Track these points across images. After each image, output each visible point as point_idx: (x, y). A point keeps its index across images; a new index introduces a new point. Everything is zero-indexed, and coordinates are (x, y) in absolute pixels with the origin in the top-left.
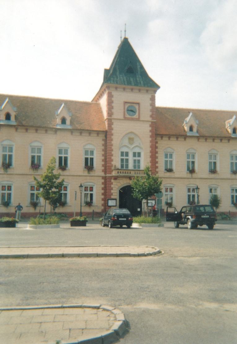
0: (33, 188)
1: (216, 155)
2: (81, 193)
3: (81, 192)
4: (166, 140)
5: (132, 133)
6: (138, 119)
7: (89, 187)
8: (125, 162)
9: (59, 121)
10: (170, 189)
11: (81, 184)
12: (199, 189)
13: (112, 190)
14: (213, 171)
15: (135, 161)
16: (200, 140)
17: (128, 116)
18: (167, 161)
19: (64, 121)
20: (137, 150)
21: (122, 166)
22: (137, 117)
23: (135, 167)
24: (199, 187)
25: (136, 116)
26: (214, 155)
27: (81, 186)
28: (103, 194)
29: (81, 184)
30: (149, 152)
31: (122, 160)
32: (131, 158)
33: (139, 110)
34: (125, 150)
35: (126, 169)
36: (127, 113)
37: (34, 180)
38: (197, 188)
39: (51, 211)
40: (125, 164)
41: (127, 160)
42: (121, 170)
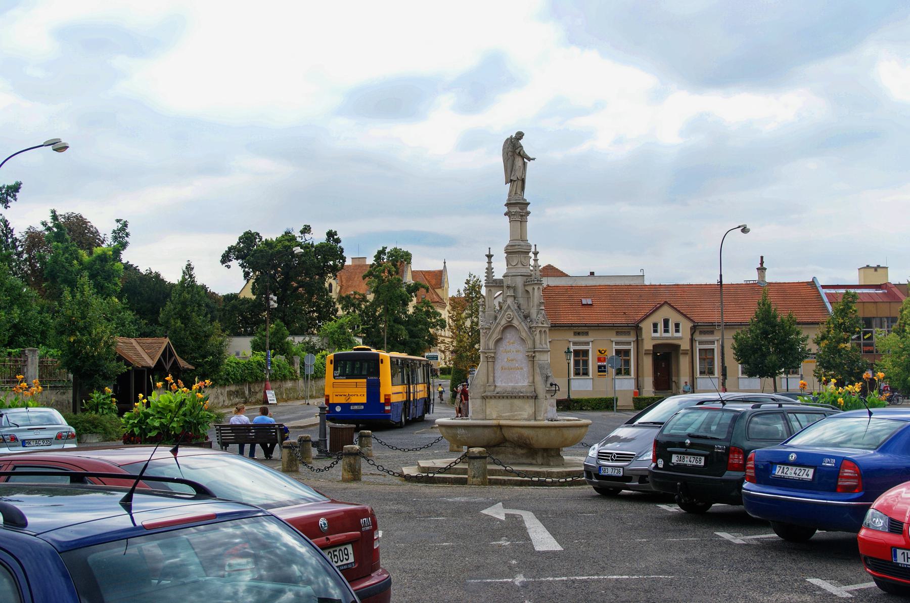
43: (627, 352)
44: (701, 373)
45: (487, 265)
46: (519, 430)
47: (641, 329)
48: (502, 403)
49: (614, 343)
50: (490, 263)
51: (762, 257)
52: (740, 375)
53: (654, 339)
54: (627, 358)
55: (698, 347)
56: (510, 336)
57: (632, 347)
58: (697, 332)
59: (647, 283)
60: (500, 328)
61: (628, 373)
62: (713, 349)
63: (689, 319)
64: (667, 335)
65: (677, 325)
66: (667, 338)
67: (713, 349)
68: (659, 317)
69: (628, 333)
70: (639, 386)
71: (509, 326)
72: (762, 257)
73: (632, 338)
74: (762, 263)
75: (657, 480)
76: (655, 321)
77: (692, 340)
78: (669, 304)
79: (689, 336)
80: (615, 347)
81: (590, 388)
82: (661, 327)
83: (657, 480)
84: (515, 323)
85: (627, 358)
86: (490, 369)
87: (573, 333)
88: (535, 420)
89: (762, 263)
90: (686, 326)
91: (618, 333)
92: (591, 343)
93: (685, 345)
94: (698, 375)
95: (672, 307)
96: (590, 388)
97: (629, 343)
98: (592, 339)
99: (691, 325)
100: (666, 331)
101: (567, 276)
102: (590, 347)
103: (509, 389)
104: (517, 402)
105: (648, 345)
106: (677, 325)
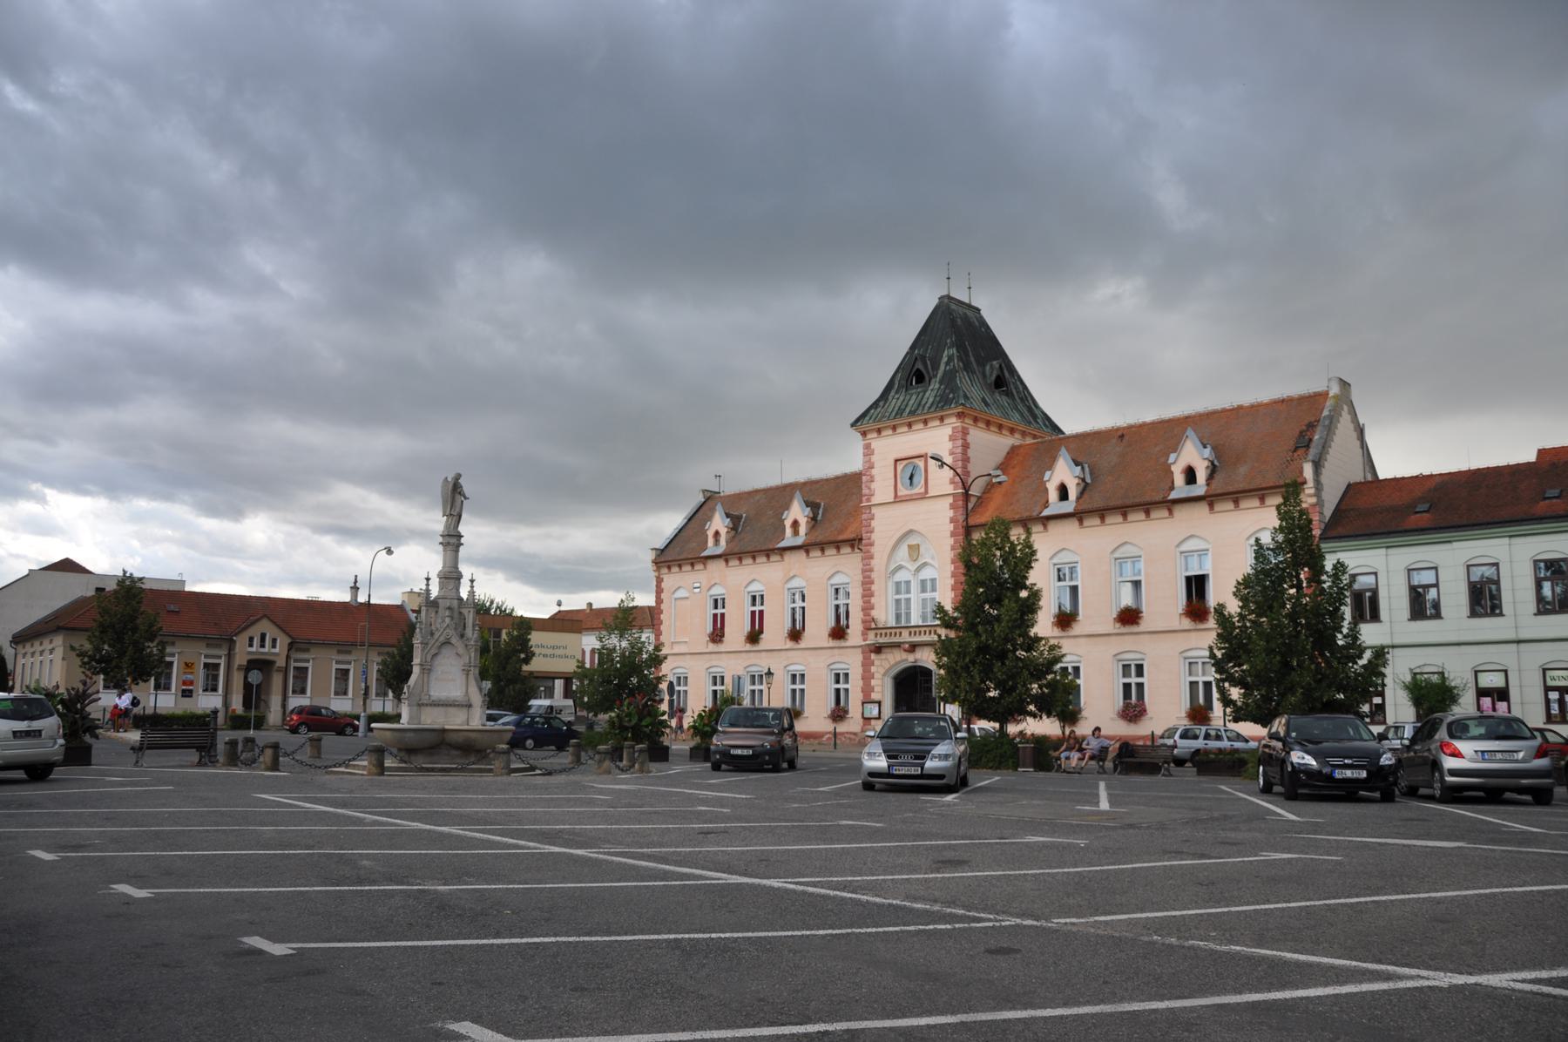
0: (298, 689)
1: (1075, 565)
2: (769, 689)
4: (763, 563)
5: (910, 532)
6: (923, 497)
7: (1133, 664)
8: (901, 608)
9: (1179, 479)
10: (191, 691)
11: (769, 669)
12: (773, 674)
13: (873, 678)
14: (795, 635)
16: (1086, 523)
19: (1063, 493)
22: (923, 490)
24: (772, 671)
25: (919, 489)
26: (1069, 565)
29: (769, 669)
30: (950, 575)
33: (926, 471)
38: (769, 673)
39: (1063, 733)
41: (908, 601)
42: (895, 628)
43: (217, 666)
44: (294, 692)
45: (469, 589)
46: (466, 734)
47: (234, 642)
48: (436, 710)
49: (334, 662)
50: (472, 587)
51: (356, 576)
52: (332, 696)
53: (250, 653)
54: (216, 673)
55: (293, 664)
56: (446, 651)
57: (222, 662)
58: (293, 650)
59: (187, 589)
60: (438, 644)
61: (215, 689)
62: (307, 668)
63: (287, 634)
64: (262, 650)
65: (274, 641)
66: (262, 653)
67: (307, 668)
68: (255, 631)
69: (219, 646)
70: (226, 703)
71: (447, 643)
72: (356, 576)
73: (223, 652)
74: (356, 582)
75: (1046, 727)
76: (251, 635)
77: (288, 657)
78: (269, 618)
79: (286, 653)
80: (203, 660)
81: (172, 704)
82: (256, 641)
83: (1046, 727)
84: (454, 641)
85: (216, 673)
86: (425, 680)
87: (205, 645)
88: (468, 725)
89: (356, 582)
90: (283, 642)
91: (208, 645)
92: (311, 661)
93: (281, 662)
94: (374, 697)
95: (272, 621)
96: (172, 704)
97: (220, 657)
98: (313, 656)
99: (290, 641)
100: (263, 646)
101: (90, 573)
102: (310, 665)
103: (443, 698)
104: (452, 710)
105: (240, 659)
106: (274, 641)
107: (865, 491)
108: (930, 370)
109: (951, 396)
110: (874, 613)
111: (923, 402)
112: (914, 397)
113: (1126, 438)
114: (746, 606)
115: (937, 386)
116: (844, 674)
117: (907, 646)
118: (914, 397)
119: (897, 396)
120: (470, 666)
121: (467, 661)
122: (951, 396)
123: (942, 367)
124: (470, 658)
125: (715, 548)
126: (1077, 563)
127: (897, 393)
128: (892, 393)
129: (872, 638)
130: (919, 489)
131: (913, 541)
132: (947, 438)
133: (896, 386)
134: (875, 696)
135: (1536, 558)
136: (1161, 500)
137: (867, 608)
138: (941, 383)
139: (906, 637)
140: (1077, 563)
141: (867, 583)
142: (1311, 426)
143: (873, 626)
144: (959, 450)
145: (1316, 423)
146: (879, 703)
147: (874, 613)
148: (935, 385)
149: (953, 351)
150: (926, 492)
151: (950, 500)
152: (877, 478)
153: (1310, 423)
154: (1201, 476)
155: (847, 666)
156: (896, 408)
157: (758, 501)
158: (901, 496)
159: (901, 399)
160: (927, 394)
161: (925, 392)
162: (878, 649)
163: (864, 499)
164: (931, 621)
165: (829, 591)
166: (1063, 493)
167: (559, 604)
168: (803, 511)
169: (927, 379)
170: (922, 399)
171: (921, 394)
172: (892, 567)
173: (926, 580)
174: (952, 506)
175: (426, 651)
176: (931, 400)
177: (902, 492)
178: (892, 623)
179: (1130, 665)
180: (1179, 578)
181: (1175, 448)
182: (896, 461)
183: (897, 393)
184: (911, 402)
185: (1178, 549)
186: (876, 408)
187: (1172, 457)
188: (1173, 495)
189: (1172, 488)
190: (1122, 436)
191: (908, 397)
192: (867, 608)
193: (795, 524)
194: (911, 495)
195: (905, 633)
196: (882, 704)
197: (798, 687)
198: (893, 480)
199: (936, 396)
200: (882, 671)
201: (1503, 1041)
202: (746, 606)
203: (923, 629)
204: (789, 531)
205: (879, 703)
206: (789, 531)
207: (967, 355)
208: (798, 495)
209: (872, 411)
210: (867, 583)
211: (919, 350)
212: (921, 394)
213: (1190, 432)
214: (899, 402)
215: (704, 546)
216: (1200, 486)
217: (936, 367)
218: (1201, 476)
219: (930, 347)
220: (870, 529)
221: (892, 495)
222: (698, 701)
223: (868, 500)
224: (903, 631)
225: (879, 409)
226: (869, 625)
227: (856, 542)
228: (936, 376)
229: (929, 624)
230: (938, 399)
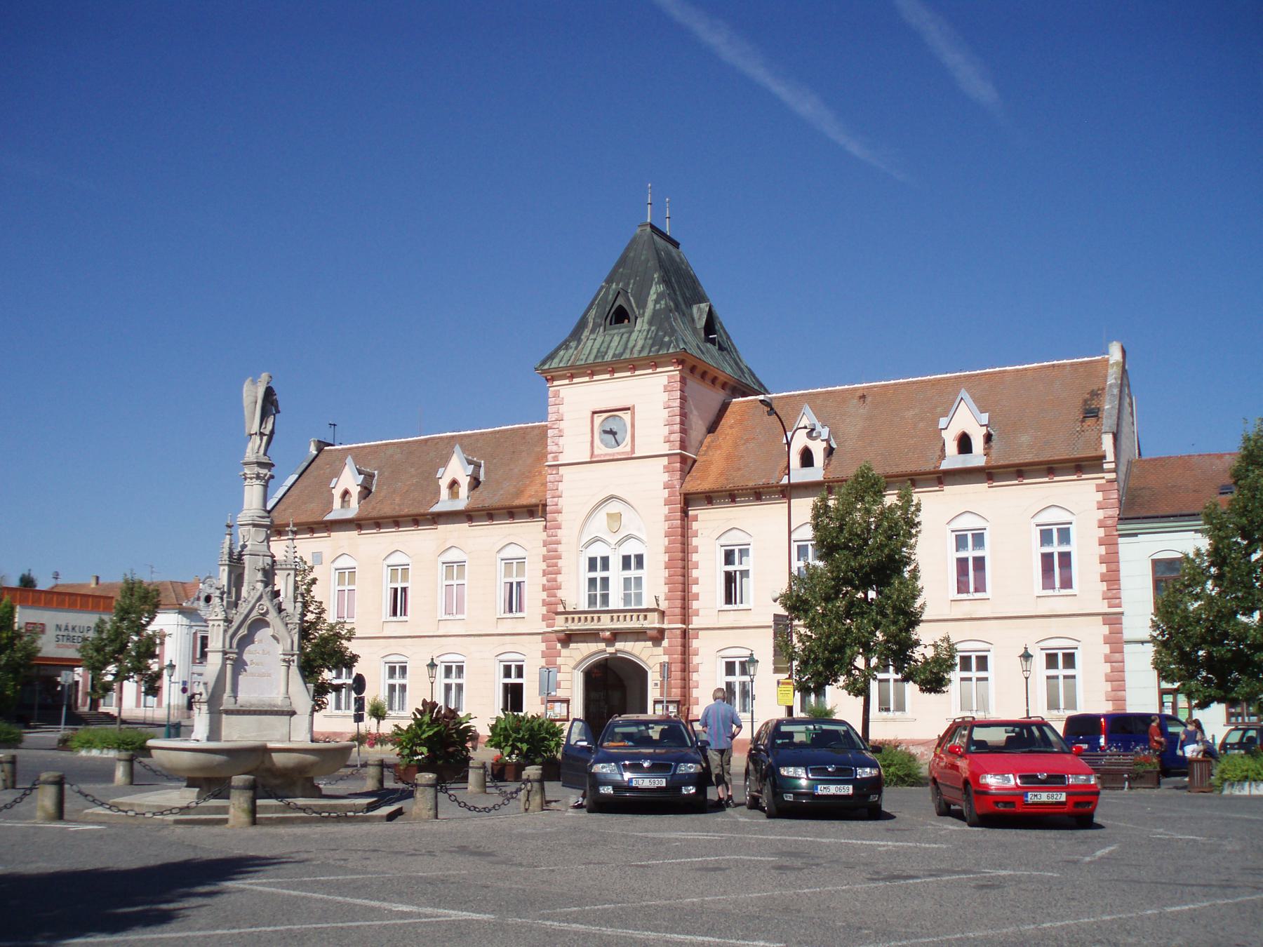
3: (432, 680)
9: (951, 447)
15: (627, 581)
17: (601, 450)
18: (1051, 555)
20: (631, 549)
21: (592, 599)
22: (628, 449)
23: (627, 598)
24: (755, 657)
25: (624, 448)
27: (432, 665)
28: (1108, 660)
31: (592, 582)
32: (616, 574)
33: (633, 426)
34: (598, 551)
35: (590, 609)
36: (602, 441)
37: (210, 655)
40: (599, 592)
41: (605, 581)
107: (551, 448)
108: (635, 309)
109: (667, 339)
110: (561, 594)
111: (630, 345)
112: (616, 339)
113: (869, 399)
114: (439, 580)
115: (646, 327)
116: (516, 666)
117: (608, 634)
118: (616, 339)
119: (593, 336)
120: (293, 655)
121: (289, 647)
122: (667, 339)
123: (650, 305)
124: (292, 642)
125: (343, 510)
126: (1071, 523)
127: (592, 331)
128: (586, 333)
129: (560, 624)
130: (624, 448)
131: (614, 507)
132: (662, 389)
133: (591, 325)
134: (561, 693)
135: (1155, 557)
136: (932, 470)
137: (551, 588)
138: (650, 323)
139: (606, 623)
140: (1071, 523)
141: (552, 560)
142: (1095, 394)
143: (561, 609)
144: (677, 403)
145: (1099, 392)
146: (567, 701)
147: (561, 594)
148: (641, 325)
149: (661, 288)
150: (633, 451)
151: (665, 461)
152: (566, 433)
153: (1093, 391)
154: (978, 444)
155: (521, 657)
156: (595, 351)
157: (392, 456)
158: (598, 456)
159: (599, 340)
160: (634, 336)
161: (631, 333)
162: (568, 638)
163: (550, 456)
164: (635, 605)
165: (332, 577)
166: (965, 444)
167: (56, 576)
168: (465, 469)
169: (632, 318)
170: (628, 341)
171: (625, 336)
172: (585, 539)
173: (630, 556)
174: (667, 469)
175: (231, 632)
176: (640, 343)
177: (601, 450)
178: (584, 606)
179: (1056, 655)
180: (439, 586)
181: (948, 410)
182: (594, 413)
183: (592, 331)
184: (614, 344)
185: (385, 562)
186: (567, 349)
187: (943, 422)
188: (945, 465)
189: (943, 456)
190: (863, 397)
191: (608, 339)
192: (551, 588)
193: (454, 484)
194: (614, 454)
195: (605, 618)
196: (571, 703)
197: (397, 681)
198: (590, 435)
199: (646, 339)
200: (573, 663)
201: (575, 946)
202: (439, 580)
203: (589, 616)
204: (445, 492)
205: (567, 701)
206: (445, 492)
207: (675, 294)
208: (349, 460)
209: (562, 353)
210: (552, 560)
211: (617, 284)
212: (625, 336)
213: (964, 393)
214: (597, 345)
215: (329, 507)
216: (976, 456)
217: (642, 304)
218: (978, 444)
219: (632, 281)
220: (558, 493)
221: (588, 453)
222: (1060, 728)
223: (555, 459)
224: (602, 616)
225: (571, 351)
226: (553, 609)
227: (535, 511)
228: (643, 315)
229: (633, 607)
230: (650, 342)
